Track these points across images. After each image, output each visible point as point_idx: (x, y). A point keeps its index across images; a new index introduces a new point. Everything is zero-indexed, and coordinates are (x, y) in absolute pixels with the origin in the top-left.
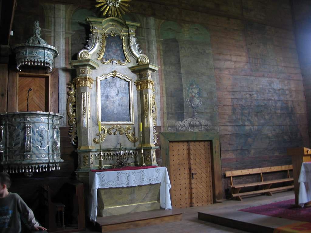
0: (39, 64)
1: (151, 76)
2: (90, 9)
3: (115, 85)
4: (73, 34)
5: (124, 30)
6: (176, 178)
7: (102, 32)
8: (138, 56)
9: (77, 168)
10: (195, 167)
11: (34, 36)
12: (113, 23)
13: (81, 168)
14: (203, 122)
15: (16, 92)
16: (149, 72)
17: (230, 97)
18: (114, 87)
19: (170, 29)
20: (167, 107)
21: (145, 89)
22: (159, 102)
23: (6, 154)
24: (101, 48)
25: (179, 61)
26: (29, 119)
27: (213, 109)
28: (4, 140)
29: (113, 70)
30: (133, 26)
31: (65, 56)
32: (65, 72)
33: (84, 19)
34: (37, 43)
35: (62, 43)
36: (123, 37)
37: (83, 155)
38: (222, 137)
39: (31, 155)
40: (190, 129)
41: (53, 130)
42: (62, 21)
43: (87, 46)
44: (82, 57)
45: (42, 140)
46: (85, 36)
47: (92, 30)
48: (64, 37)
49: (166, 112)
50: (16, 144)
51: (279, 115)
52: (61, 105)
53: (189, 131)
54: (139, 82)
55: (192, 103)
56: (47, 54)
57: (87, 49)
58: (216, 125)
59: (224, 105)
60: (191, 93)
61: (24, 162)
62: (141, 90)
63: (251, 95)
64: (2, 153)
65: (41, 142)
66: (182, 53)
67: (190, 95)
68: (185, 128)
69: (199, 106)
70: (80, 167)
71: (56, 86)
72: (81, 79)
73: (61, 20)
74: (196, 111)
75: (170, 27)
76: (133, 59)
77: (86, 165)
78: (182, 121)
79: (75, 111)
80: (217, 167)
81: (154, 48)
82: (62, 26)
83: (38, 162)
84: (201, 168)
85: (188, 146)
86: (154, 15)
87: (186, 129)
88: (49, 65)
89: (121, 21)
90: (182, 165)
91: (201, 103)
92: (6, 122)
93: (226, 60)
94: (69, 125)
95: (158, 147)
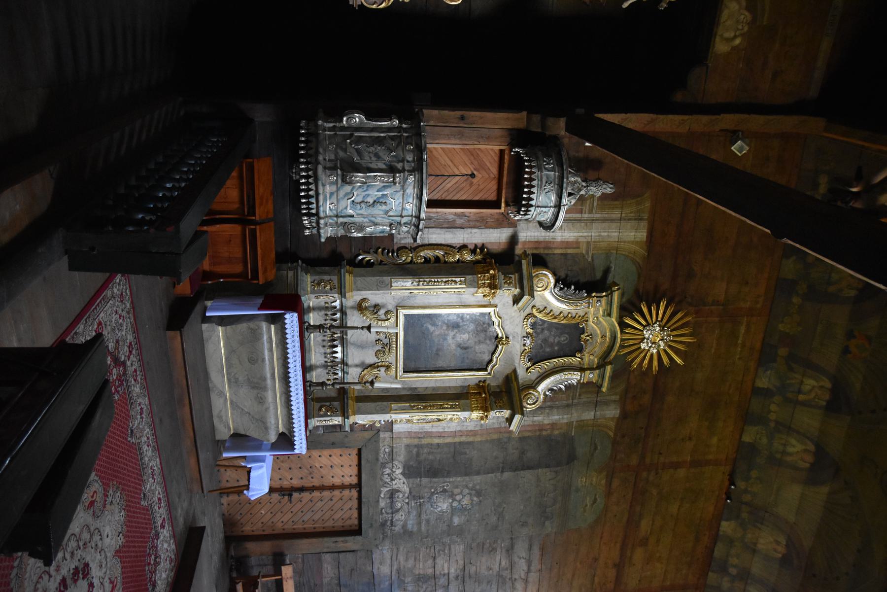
0: (525, 196)
1: (497, 415)
2: (636, 291)
3: (480, 342)
4: (586, 257)
5: (593, 361)
6: (282, 462)
7: (591, 316)
8: (542, 387)
9: (307, 264)
10: (304, 501)
11: (584, 184)
12: (608, 339)
13: (306, 274)
14: (400, 517)
15: (467, 143)
16: (507, 413)
17: (452, 570)
18: (476, 340)
19: (596, 448)
20: (432, 444)
21: (472, 405)
22: (444, 428)
24: (558, 314)
25: (529, 468)
26: (411, 179)
28: (368, 126)
29: (511, 338)
30: (602, 377)
31: (542, 240)
33: (616, 280)
34: (570, 190)
35: (568, 235)
36: (579, 358)
37: (335, 279)
38: (369, 554)
39: (336, 182)
40: (384, 490)
41: (389, 224)
42: (614, 234)
43: (562, 286)
44: (538, 277)
45: (368, 204)
46: (583, 279)
47: (594, 297)
49: (423, 443)
50: (358, 151)
52: (439, 234)
53: (382, 489)
54: (486, 391)
55: (441, 495)
56: (545, 212)
57: (555, 286)
59: (434, 558)
60: (461, 493)
61: (320, 168)
62: (469, 395)
64: (342, 121)
65: (363, 202)
66: (545, 474)
67: (456, 491)
68: (388, 480)
69: (434, 508)
70: (309, 272)
71: (482, 224)
72: (493, 277)
73: (615, 232)
74: (424, 502)
75: (599, 448)
76: (534, 378)
77: (312, 285)
78: (403, 474)
79: (427, 260)
80: (305, 545)
81: (556, 417)
82: (603, 234)
83: (321, 198)
84: (302, 512)
86: (624, 415)
87: (386, 483)
88: (522, 215)
89: (613, 354)
90: (311, 473)
91: (439, 512)
92: (405, 130)
93: (529, 563)
94: (399, 249)
95: (347, 429)
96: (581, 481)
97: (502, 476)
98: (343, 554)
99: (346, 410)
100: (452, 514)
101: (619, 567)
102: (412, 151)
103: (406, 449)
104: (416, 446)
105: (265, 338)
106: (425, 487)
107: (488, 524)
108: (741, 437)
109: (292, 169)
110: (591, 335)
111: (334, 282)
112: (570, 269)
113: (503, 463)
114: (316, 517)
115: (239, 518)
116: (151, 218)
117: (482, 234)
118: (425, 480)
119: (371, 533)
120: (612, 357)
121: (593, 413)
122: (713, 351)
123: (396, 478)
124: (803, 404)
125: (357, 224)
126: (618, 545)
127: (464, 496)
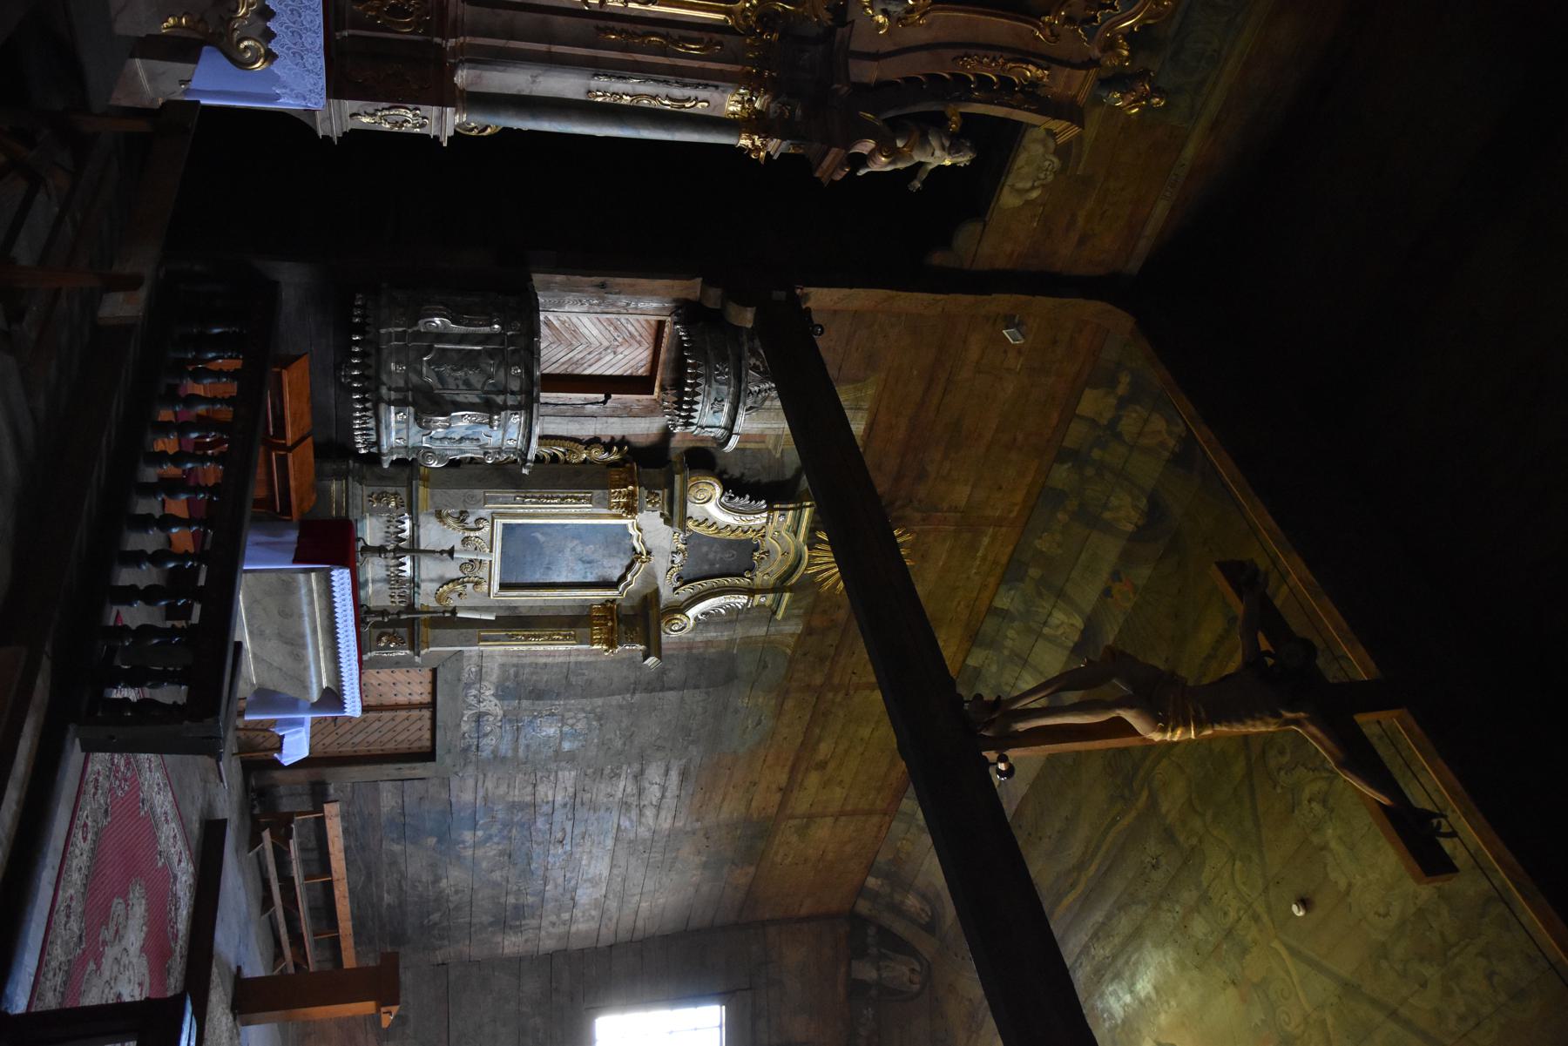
0: (687, 389)
8: (693, 612)
19: (765, 667)
20: (536, 664)
21: (592, 635)
23: (415, 340)
27: (525, 763)
32: (661, 431)
35: (750, 426)
36: (748, 578)
38: (446, 784)
40: (468, 713)
48: (767, 432)
51: (502, 900)
52: (560, 423)
53: (465, 712)
58: (477, 769)
59: (535, 786)
63: (561, 842)
66: (694, 698)
68: (474, 702)
71: (626, 412)
72: (631, 495)
75: (770, 666)
77: (370, 501)
85: (421, 704)
86: (809, 631)
87: (471, 705)
89: (794, 579)
93: (664, 789)
96: (743, 702)
97: (632, 698)
98: (409, 782)
99: (416, 642)
100: (562, 739)
101: (786, 791)
102: (518, 376)
103: (500, 668)
104: (514, 665)
105: (304, 591)
106: (525, 710)
107: (609, 748)
108: (964, 660)
109: (341, 370)
110: (768, 552)
111: (402, 496)
112: (748, 466)
113: (635, 683)
114: (371, 739)
115: (261, 741)
116: (173, 626)
117: (622, 424)
118: (525, 703)
119: (448, 760)
120: (794, 581)
121: (765, 629)
122: (941, 563)
123: (484, 700)
124: (1049, 639)
125: (437, 453)
126: (787, 769)
127: (578, 720)
